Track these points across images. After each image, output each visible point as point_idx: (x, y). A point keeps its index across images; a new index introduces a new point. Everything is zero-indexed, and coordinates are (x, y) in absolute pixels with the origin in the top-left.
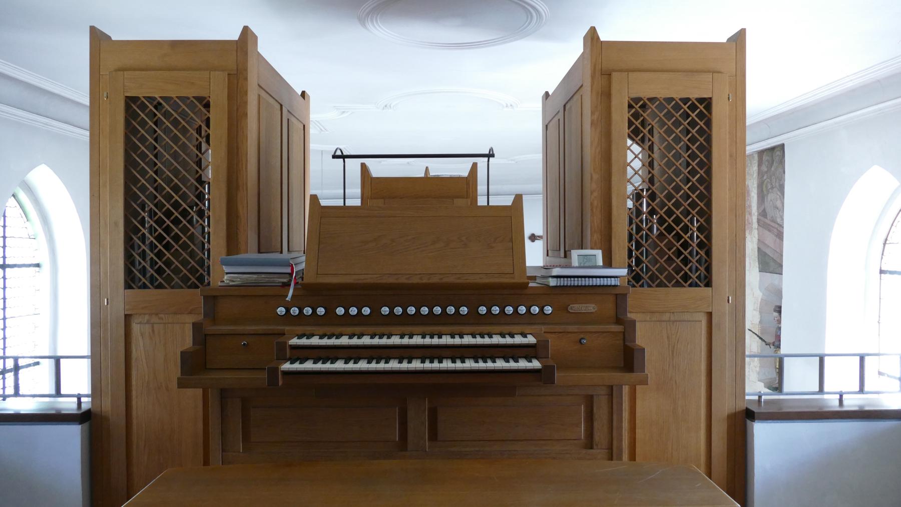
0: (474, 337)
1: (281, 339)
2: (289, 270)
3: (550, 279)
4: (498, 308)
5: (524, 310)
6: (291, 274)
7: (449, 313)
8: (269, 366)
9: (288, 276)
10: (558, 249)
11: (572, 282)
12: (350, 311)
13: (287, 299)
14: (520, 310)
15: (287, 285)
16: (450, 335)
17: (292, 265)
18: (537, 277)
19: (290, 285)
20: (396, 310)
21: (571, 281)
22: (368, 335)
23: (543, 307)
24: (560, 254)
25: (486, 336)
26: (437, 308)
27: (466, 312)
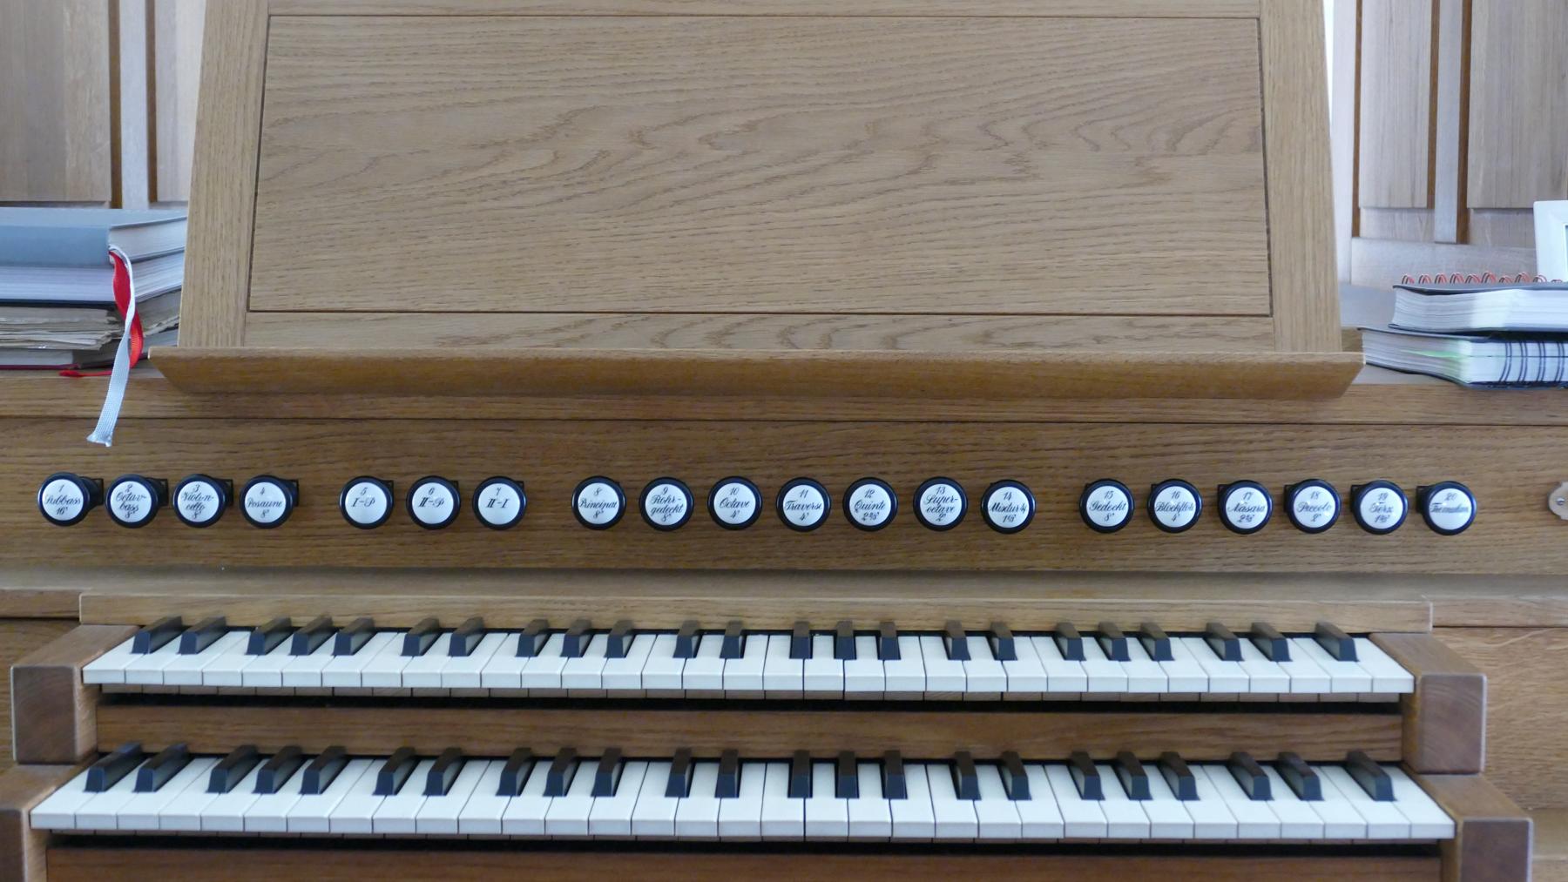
0: (1073, 653)
1: (48, 654)
2: (104, 290)
3: (1466, 348)
4: (1186, 496)
5: (882, 506)
6: (115, 309)
9: (101, 316)
10: (1422, 201)
13: (94, 437)
14: (1306, 508)
15: (96, 363)
16: (943, 634)
17: (120, 262)
18: (1365, 336)
19: (108, 366)
20: (657, 500)
21: (1543, 356)
22: (509, 631)
23: (1223, 492)
24: (1430, 230)
25: (977, 645)
26: (869, 494)
27: (1021, 517)
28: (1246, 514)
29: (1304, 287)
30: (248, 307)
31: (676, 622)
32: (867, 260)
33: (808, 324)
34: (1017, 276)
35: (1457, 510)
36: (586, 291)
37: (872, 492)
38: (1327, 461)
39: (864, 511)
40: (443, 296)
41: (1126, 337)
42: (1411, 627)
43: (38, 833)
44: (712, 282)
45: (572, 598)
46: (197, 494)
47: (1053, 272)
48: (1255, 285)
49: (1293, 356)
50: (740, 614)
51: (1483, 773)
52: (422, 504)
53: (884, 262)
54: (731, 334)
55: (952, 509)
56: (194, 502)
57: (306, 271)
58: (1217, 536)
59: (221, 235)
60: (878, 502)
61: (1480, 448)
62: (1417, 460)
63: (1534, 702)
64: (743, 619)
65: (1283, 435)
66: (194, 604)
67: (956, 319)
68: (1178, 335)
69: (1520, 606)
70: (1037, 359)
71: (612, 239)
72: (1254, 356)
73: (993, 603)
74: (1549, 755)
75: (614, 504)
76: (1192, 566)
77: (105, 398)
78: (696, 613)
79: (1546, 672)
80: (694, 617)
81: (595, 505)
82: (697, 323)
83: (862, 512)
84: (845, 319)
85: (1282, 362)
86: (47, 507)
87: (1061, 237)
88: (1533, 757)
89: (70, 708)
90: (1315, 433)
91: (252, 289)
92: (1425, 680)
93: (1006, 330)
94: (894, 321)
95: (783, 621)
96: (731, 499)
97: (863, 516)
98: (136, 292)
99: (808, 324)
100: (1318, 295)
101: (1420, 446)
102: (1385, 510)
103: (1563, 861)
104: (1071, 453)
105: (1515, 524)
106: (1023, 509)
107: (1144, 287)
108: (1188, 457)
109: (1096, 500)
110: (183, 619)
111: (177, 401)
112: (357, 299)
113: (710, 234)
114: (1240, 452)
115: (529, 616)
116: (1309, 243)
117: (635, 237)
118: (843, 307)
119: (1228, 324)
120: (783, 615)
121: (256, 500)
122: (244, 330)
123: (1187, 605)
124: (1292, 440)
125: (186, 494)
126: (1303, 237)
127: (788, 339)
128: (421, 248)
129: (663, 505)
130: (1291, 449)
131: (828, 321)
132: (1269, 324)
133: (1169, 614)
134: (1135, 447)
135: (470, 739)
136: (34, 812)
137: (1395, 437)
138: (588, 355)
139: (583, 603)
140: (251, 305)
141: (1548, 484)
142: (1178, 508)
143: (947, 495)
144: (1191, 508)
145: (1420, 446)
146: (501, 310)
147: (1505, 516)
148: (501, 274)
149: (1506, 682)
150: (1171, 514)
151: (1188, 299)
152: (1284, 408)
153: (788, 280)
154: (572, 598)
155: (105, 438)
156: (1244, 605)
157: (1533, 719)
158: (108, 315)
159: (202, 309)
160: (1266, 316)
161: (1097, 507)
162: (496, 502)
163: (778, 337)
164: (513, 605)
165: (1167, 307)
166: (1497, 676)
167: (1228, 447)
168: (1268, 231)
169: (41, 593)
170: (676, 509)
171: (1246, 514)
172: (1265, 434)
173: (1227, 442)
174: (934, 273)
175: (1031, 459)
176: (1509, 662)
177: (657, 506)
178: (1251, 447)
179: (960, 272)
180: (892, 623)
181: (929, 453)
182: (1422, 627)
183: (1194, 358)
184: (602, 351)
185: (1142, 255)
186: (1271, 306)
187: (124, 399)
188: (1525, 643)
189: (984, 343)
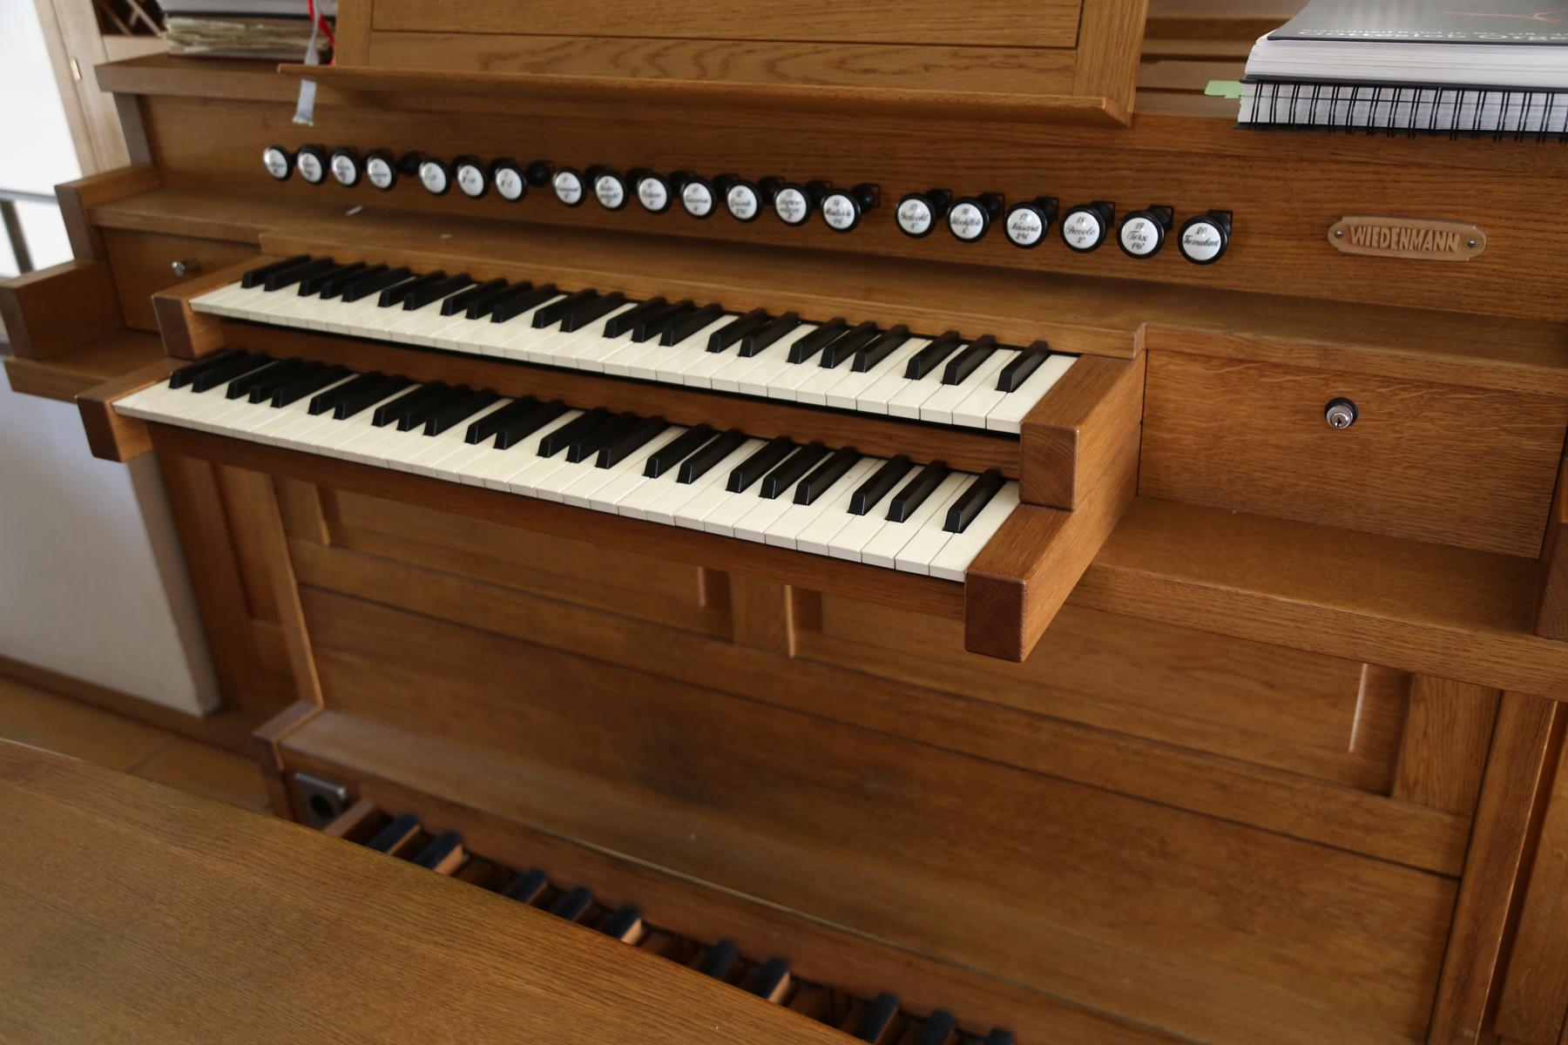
13: (298, 120)
14: (1073, 231)
28: (1022, 232)
29: (1110, 21)
34: (872, 8)
35: (1207, 243)
41: (951, 66)
42: (1117, 353)
49: (1040, 99)
61: (1269, 179)
63: (1245, 424)
68: (992, 66)
69: (1232, 342)
72: (1007, 97)
74: (1255, 471)
85: (1029, 104)
88: (1241, 470)
96: (648, 192)
100: (1121, 28)
101: (1214, 173)
103: (1178, 583)
105: (1299, 251)
114: (1055, 169)
118: (739, 34)
119: (1038, 55)
123: (933, 314)
124: (1098, 161)
130: (1100, 170)
131: (727, 46)
132: (1073, 57)
137: (1192, 164)
144: (977, 224)
145: (1214, 173)
147: (1290, 243)
151: (1007, 32)
165: (989, 38)
166: (1212, 398)
171: (1022, 232)
176: (1223, 387)
178: (1065, 165)
188: (1240, 372)
189: (839, 68)
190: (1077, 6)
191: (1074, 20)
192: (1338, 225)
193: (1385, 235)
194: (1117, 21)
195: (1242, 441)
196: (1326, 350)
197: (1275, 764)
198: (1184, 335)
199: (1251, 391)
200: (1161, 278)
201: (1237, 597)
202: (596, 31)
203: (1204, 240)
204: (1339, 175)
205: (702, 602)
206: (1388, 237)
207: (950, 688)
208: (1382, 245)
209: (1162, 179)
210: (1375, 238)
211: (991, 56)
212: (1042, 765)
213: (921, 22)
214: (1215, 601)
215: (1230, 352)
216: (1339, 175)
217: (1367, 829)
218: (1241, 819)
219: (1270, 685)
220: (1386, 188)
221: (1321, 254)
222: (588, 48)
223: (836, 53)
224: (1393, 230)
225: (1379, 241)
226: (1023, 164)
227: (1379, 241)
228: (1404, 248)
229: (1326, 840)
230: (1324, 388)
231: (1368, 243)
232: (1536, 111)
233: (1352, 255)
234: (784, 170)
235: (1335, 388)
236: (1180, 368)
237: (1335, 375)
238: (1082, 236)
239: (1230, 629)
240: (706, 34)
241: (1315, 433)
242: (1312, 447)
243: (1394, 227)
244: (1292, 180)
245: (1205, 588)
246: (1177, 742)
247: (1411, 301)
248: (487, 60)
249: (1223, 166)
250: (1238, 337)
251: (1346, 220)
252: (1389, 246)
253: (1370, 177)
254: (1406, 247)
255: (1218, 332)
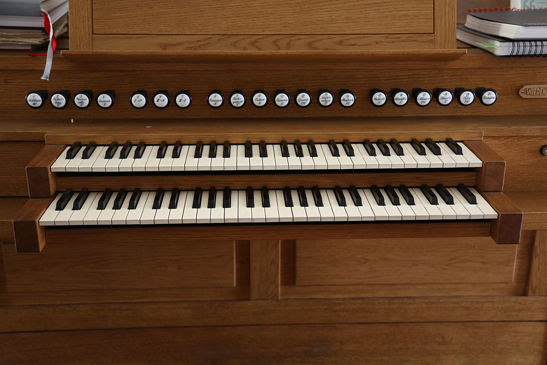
2: (40, 23)
3: (497, 43)
5: (307, 100)
6: (45, 30)
7: (323, 103)
8: (28, 167)
9: (40, 33)
11: (539, 48)
12: (155, 99)
13: (43, 78)
15: (42, 48)
20: (235, 99)
26: (303, 96)
27: (352, 103)
28: (423, 101)
29: (445, 23)
30: (93, 32)
31: (243, 141)
32: (301, 16)
33: (282, 39)
34: (351, 21)
36: (209, 27)
37: (304, 95)
38: (448, 80)
39: (301, 102)
40: (160, 29)
43: (41, 227)
44: (250, 24)
45: (209, 134)
46: (81, 98)
47: (362, 19)
48: (429, 23)
49: (443, 51)
50: (264, 138)
51: (503, 192)
52: (158, 101)
53: (307, 17)
54: (257, 42)
55: (329, 100)
56: (80, 101)
57: (113, 20)
58: (411, 105)
59: (81, 6)
60: (306, 99)
61: (498, 75)
62: (477, 79)
64: (265, 140)
65: (435, 72)
66: (84, 138)
67: (331, 36)
68: (403, 41)
69: (511, 130)
70: (359, 53)
71: (216, 9)
72: (430, 51)
73: (344, 133)
74: (515, 175)
75: (221, 100)
76: (403, 114)
77: (46, 64)
78: (250, 138)
79: (516, 150)
80: (249, 140)
81: (215, 101)
82: (246, 39)
83: (301, 102)
84: (294, 36)
86: (29, 103)
87: (365, 7)
89: (48, 180)
90: (445, 71)
91: (94, 26)
92: (486, 163)
93: (347, 40)
94: (311, 37)
95: (277, 140)
96: (259, 98)
97: (301, 103)
98: (51, 23)
99: (282, 39)
101: (479, 75)
102: (468, 99)
104: (366, 79)
105: (507, 99)
106: (352, 100)
107: (392, 24)
108: (404, 80)
109: (376, 97)
110: (81, 142)
111: (71, 65)
112: (131, 30)
113: (249, 7)
114: (420, 78)
115: (196, 140)
116: (447, 7)
117: (224, 8)
118: (293, 32)
119: (420, 36)
120: (277, 138)
121: (101, 100)
122: (92, 41)
124: (437, 74)
125: (77, 98)
126: (445, 6)
127: (276, 44)
128: (151, 12)
129: (236, 101)
130: (437, 77)
131: (289, 37)
132: (433, 36)
133: (400, 136)
134: (387, 77)
135: (181, 185)
136: (40, 221)
138: (212, 53)
139: (213, 135)
140: (94, 32)
141: (519, 86)
142: (402, 99)
143: (328, 96)
145: (479, 75)
146: (180, 34)
148: (179, 21)
149: (504, 153)
150: (400, 101)
151: (407, 28)
152: (436, 64)
153: (275, 23)
154: (209, 134)
155: (47, 78)
156: (424, 133)
157: (511, 164)
158: (43, 32)
159: (77, 33)
160: (432, 33)
161: (376, 99)
162: (182, 100)
163: (273, 43)
164: (190, 137)
165: (400, 31)
166: (501, 152)
167: (416, 76)
168: (434, 4)
169: (31, 133)
170: (241, 102)
172: (429, 72)
173: (416, 75)
174: (323, 20)
175: (353, 81)
176: (505, 147)
177: (235, 101)
178: (424, 76)
179: (332, 20)
180: (312, 141)
181: (320, 80)
182: (480, 139)
183: (411, 52)
184: (217, 52)
185: (392, 13)
186: (434, 30)
187: (52, 64)
188: (511, 141)
190: (432, 18)
191: (432, 23)
192: (523, 89)
193: (538, 91)
194: (447, 23)
195: (511, 165)
196: (542, 129)
197: (485, 294)
198: (494, 130)
199: (515, 147)
200: (459, 114)
201: (544, 215)
202: (223, 32)
203: (490, 97)
204: (521, 72)
205: (235, 285)
206: (539, 91)
207: (352, 296)
208: (537, 94)
209: (460, 78)
210: (535, 92)
211: (402, 37)
212: (394, 319)
213: (372, 26)
214: (536, 218)
215: (510, 134)
216: (521, 72)
217: (520, 310)
218: (473, 320)
219: (484, 263)
220: (536, 75)
221: (515, 100)
222: (219, 40)
223: (338, 38)
224: (541, 89)
225: (536, 93)
226: (408, 77)
227: (536, 93)
228: (544, 94)
229: (505, 319)
230: (540, 142)
231: (532, 94)
232: (539, 48)
233: (528, 99)
234: (306, 86)
235: (543, 142)
236: (490, 142)
237: (544, 137)
238: (446, 100)
239: (541, 227)
240: (278, 33)
241: (536, 158)
242: (536, 164)
243: (541, 88)
244: (506, 75)
245: (533, 214)
246: (447, 295)
247: (544, 112)
248: (165, 46)
249: (482, 72)
250: (513, 128)
251: (525, 87)
252: (539, 94)
253: (531, 72)
254: (545, 94)
255: (506, 127)
